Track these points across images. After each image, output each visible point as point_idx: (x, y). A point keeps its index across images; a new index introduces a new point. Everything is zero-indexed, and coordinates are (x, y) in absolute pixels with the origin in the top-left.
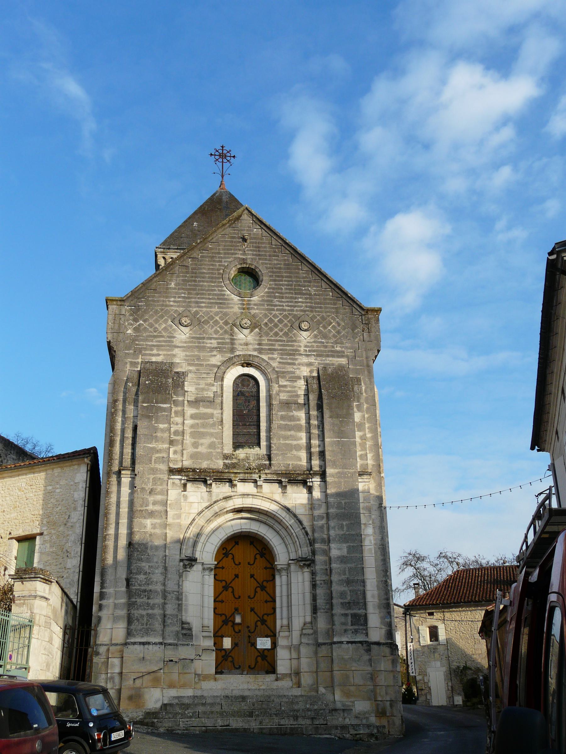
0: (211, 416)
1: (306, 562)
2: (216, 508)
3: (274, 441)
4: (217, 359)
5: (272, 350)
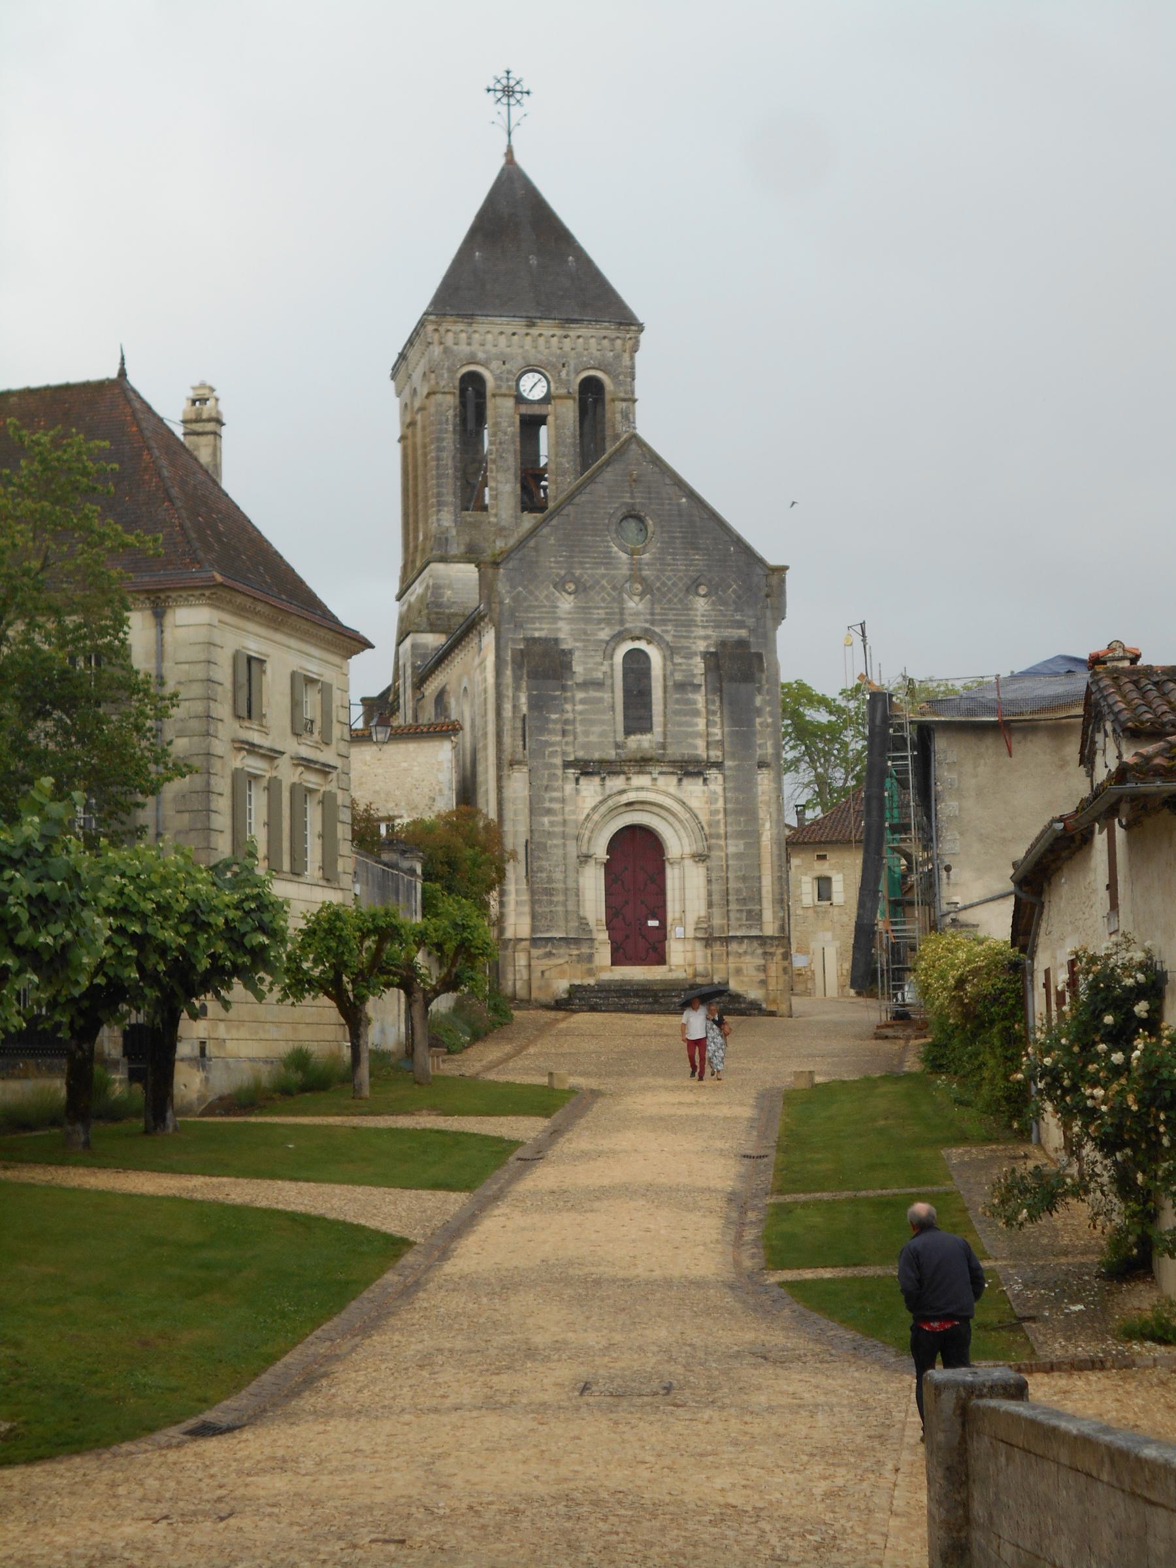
0: (601, 700)
1: (700, 858)
2: (610, 803)
4: (605, 634)
5: (664, 622)
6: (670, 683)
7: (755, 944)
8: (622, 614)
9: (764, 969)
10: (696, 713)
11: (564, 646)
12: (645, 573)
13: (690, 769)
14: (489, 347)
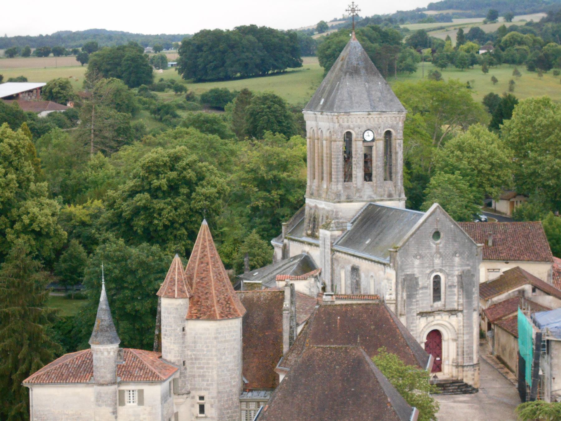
0: (427, 292)
1: (455, 340)
2: (429, 325)
3: (447, 300)
4: (428, 271)
5: (446, 266)
6: (447, 286)
7: (471, 367)
8: (433, 264)
9: (473, 375)
10: (455, 295)
11: (416, 276)
12: (440, 251)
13: (453, 312)
14: (354, 123)
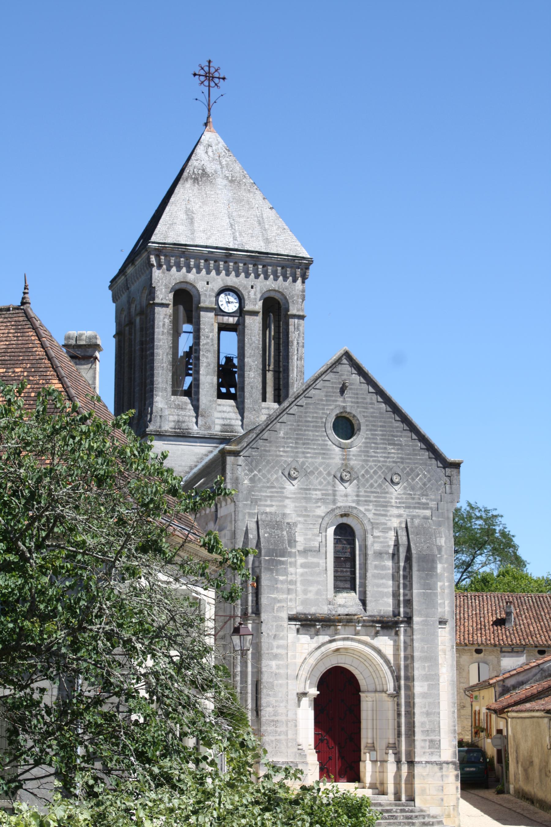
0: (318, 565)
